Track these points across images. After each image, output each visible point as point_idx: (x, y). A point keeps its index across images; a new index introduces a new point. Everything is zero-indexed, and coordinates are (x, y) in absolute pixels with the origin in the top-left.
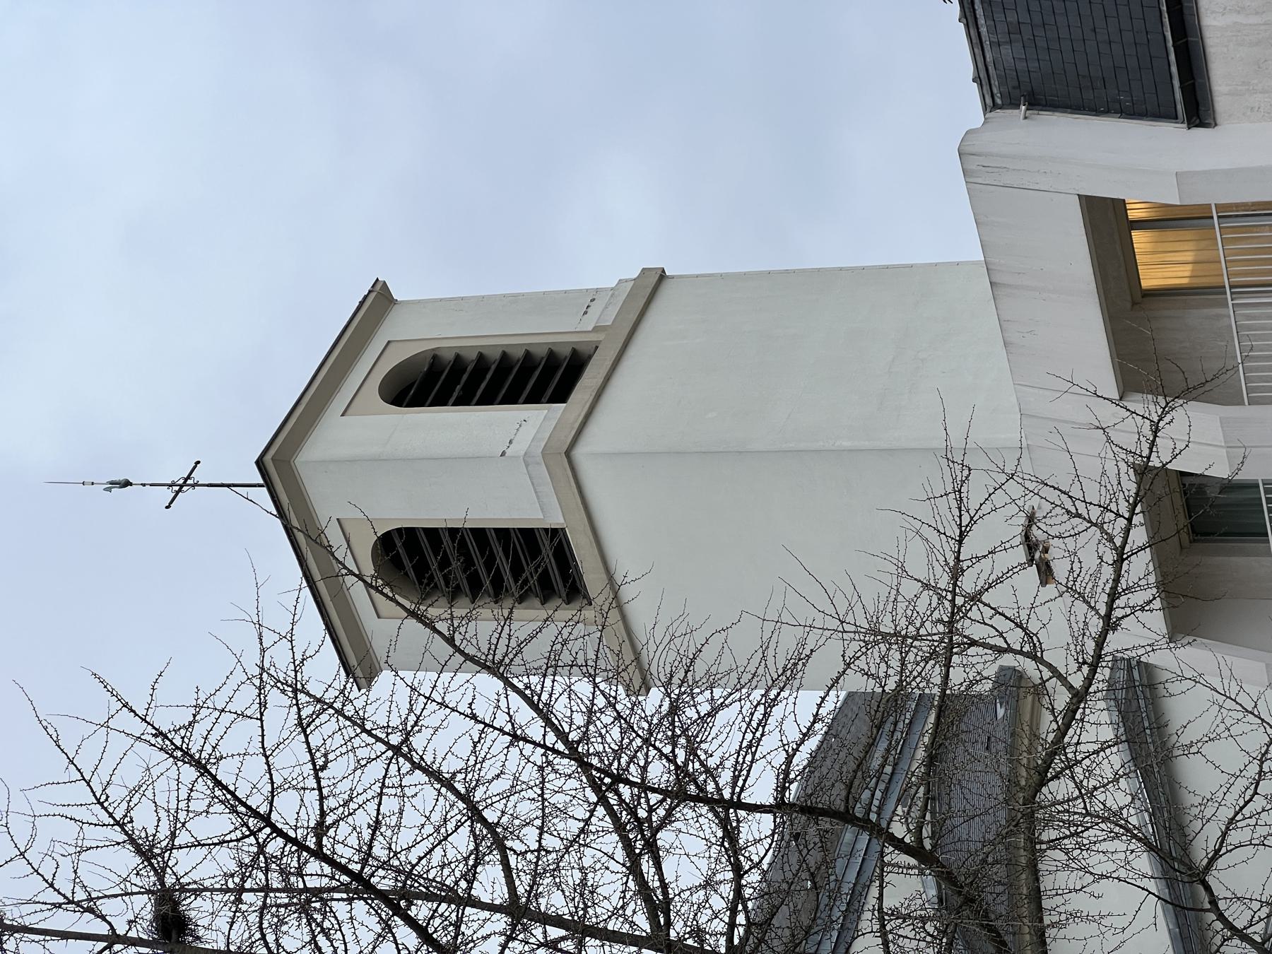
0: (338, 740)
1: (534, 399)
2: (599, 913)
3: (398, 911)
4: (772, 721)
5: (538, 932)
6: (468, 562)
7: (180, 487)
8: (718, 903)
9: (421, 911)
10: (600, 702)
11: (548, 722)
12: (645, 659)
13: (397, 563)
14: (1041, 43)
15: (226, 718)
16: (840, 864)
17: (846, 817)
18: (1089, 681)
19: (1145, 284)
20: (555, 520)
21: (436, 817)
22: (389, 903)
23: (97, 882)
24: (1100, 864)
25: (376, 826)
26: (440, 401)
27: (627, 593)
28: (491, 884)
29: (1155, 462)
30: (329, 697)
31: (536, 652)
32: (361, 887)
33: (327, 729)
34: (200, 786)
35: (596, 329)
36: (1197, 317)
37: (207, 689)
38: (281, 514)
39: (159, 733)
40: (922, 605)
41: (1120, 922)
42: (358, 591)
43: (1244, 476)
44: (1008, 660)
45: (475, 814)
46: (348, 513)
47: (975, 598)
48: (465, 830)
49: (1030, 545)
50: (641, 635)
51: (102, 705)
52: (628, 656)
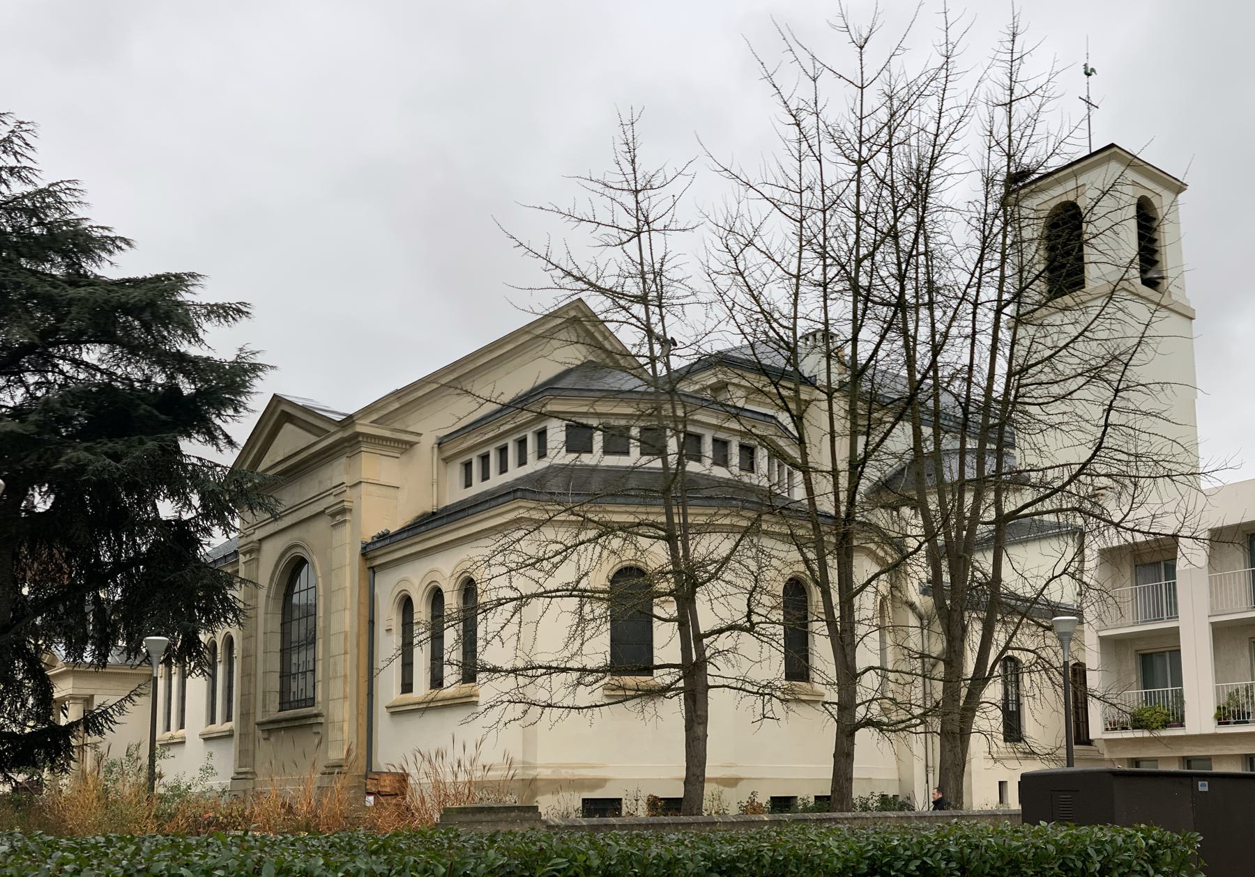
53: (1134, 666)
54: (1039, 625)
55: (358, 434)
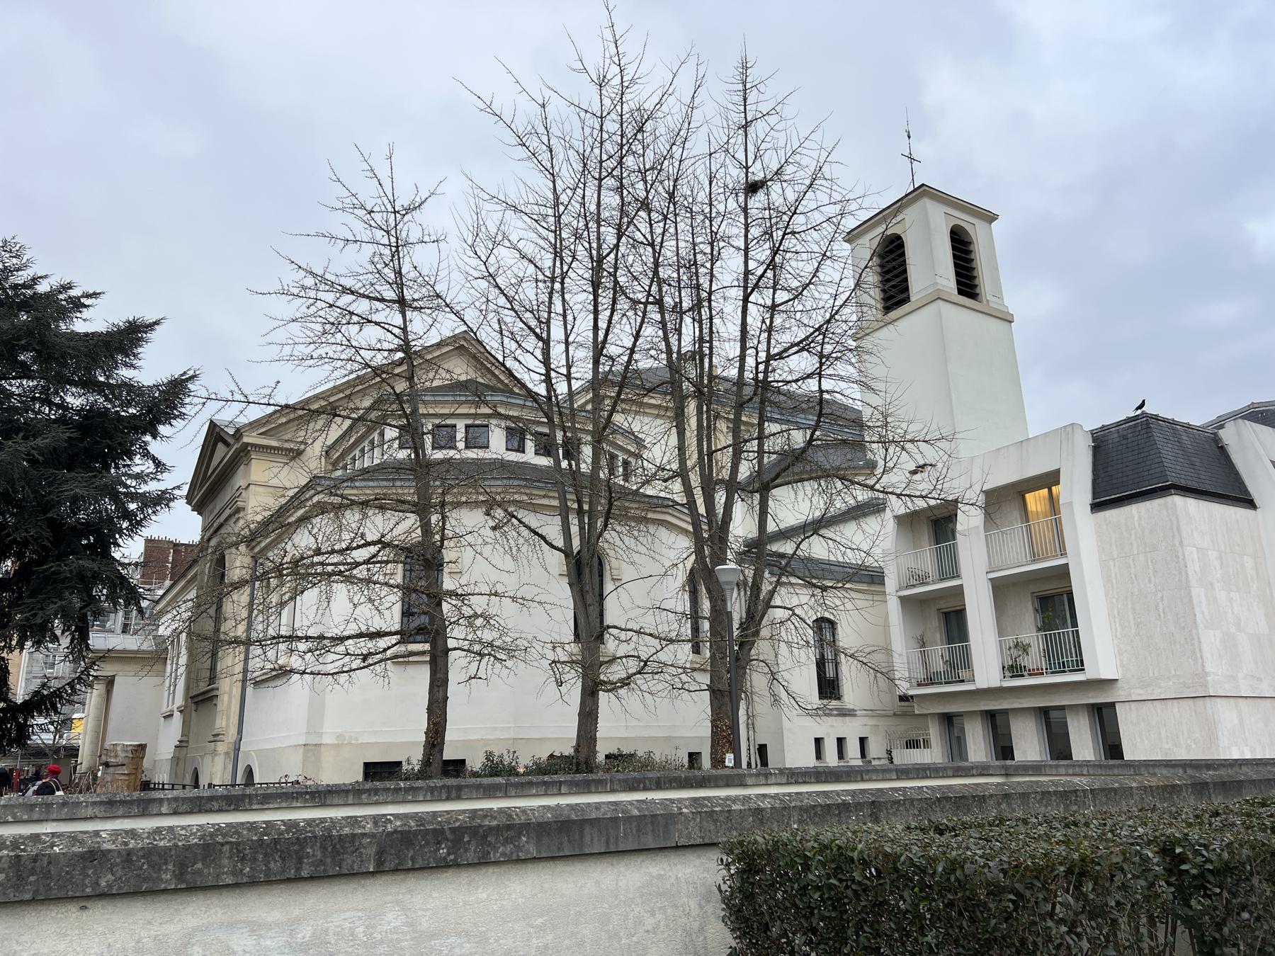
0: (826, 233)
1: (958, 282)
2: (775, 336)
3: (768, 265)
4: (852, 385)
5: (768, 316)
6: (895, 268)
7: (910, 158)
8: (785, 375)
9: (770, 274)
10: (851, 324)
11: (841, 306)
12: (867, 337)
13: (892, 242)
14: (1120, 448)
15: (829, 191)
16: (803, 416)
17: (820, 415)
18: (878, 491)
19: (1027, 495)
20: (913, 299)
21: (802, 274)
22: (771, 262)
23: (766, 158)
24: (815, 500)
25: (797, 253)
26: (954, 248)
27: (890, 327)
28: (782, 296)
29: (960, 505)
30: (840, 227)
31: (866, 299)
32: (775, 252)
33: (829, 228)
34: (804, 187)
35: (988, 301)
36: (1016, 514)
37: (838, 182)
38: (907, 195)
39: (821, 168)
40: (899, 431)
41: (796, 508)
42: (880, 229)
43: (958, 535)
44: (881, 463)
45: (805, 286)
46: (908, 223)
47: (903, 448)
48: (799, 284)
49: (923, 466)
50: (876, 335)
51: (828, 144)
52: (867, 331)
53: (937, 624)
54: (815, 586)
55: (247, 444)
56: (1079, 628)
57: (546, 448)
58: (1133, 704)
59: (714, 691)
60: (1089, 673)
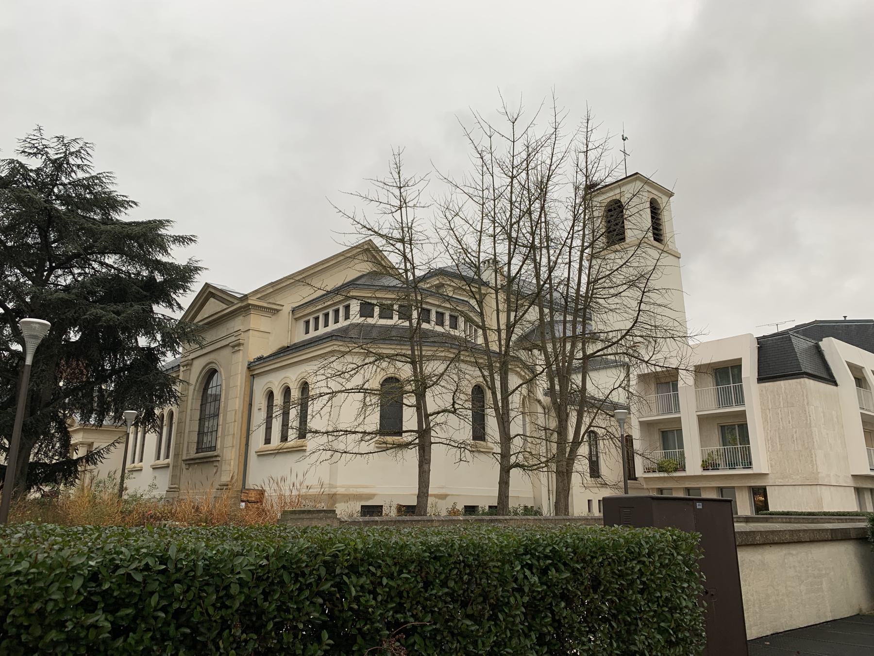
20: (628, 240)
55: (250, 305)
56: (751, 445)
57: (386, 312)
58: (776, 487)
59: (558, 473)
60: (756, 469)
